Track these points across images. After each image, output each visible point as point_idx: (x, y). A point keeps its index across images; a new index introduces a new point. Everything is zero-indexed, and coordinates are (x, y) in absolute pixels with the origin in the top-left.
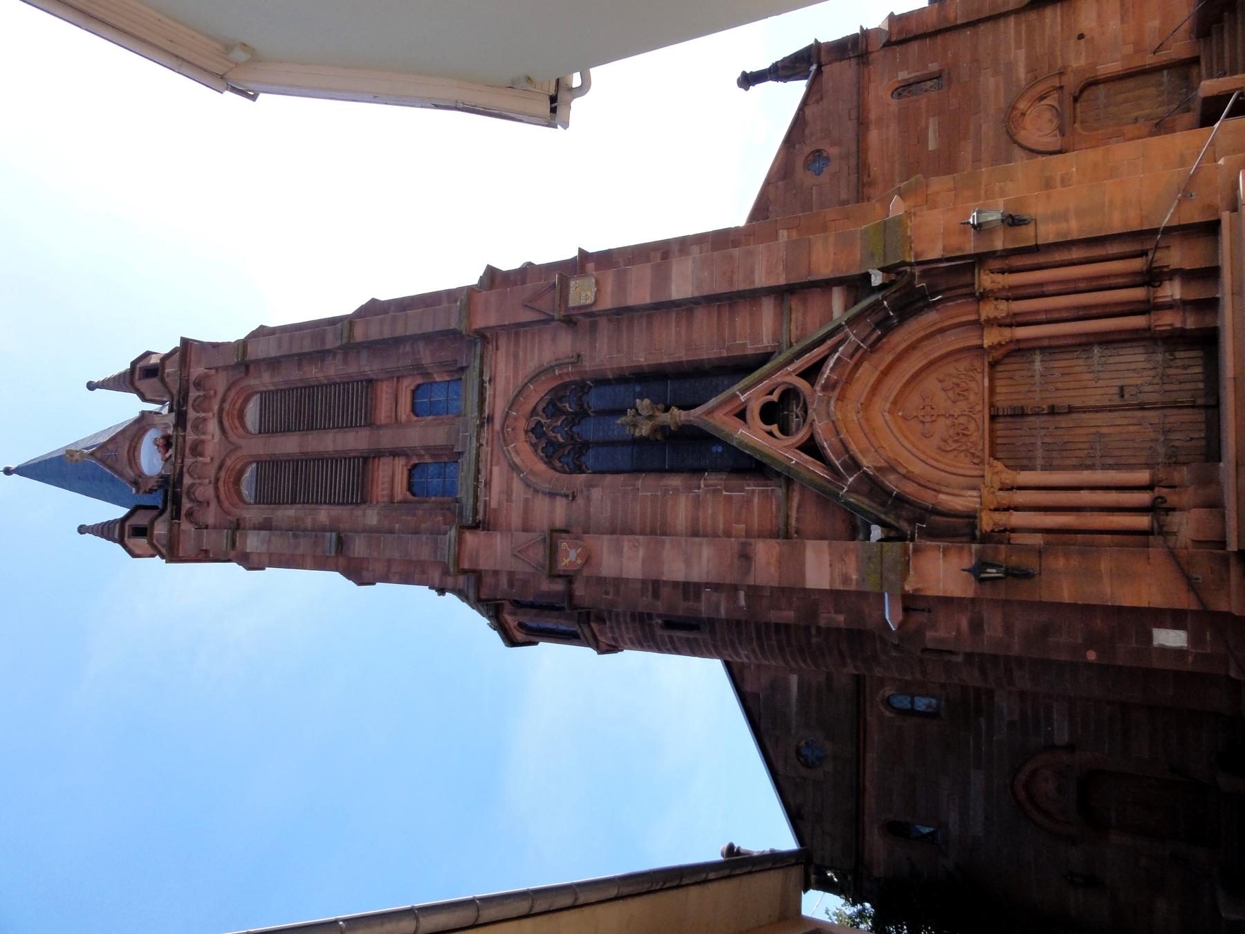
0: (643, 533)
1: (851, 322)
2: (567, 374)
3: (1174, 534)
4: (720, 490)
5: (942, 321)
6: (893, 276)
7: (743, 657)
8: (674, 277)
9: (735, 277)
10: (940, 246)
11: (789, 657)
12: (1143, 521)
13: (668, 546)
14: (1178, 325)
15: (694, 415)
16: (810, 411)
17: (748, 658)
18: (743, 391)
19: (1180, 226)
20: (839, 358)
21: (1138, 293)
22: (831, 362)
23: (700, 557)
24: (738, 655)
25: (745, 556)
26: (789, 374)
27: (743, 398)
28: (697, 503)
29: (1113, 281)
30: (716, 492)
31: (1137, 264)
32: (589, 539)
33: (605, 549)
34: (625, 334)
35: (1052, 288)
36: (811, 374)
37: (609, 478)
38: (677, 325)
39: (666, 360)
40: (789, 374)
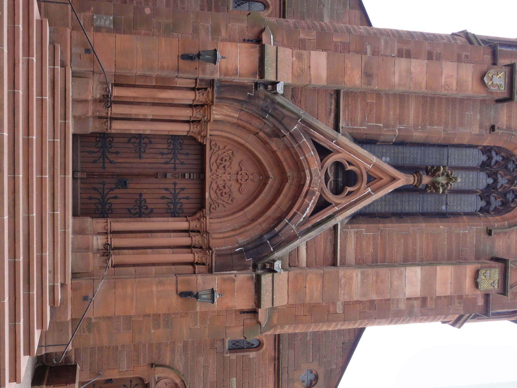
0: (440, 99)
1: (293, 238)
2: (498, 221)
4: (385, 126)
5: (234, 236)
7: (362, 29)
8: (419, 284)
9: (375, 278)
11: (332, 28)
12: (117, 92)
13: (424, 85)
16: (323, 177)
17: (360, 28)
18: (369, 195)
20: (303, 214)
21: (116, 242)
22: (308, 211)
23: (400, 76)
24: (366, 29)
25: (368, 75)
26: (337, 204)
27: (369, 190)
28: (401, 119)
30: (387, 126)
32: (482, 94)
33: (470, 83)
36: (322, 205)
38: (415, 251)
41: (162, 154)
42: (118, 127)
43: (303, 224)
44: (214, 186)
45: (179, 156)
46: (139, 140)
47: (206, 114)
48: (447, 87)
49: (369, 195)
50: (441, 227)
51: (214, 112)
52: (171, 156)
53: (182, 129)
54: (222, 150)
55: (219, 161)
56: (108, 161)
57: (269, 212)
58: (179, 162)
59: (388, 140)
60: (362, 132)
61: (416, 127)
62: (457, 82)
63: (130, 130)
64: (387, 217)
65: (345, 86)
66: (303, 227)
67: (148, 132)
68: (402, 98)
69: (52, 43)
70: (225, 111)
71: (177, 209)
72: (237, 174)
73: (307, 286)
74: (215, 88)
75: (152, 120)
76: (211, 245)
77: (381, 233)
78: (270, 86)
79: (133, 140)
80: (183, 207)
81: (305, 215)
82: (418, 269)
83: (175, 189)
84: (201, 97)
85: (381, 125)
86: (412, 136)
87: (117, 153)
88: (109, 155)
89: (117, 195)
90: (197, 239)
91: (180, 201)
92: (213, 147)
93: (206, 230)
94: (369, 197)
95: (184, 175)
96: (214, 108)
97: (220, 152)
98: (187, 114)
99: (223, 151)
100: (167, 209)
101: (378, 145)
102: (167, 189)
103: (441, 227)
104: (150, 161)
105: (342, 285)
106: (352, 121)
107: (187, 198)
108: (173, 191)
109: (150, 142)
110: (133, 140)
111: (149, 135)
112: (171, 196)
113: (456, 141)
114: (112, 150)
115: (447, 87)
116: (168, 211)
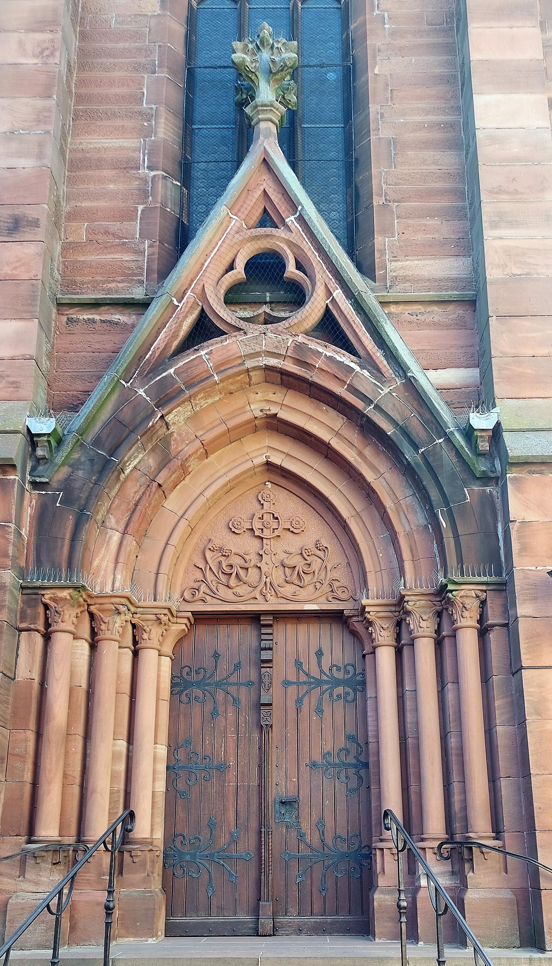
3: (23, 873)
6: (484, 446)
10: (530, 517)
13: (40, 103)
14: (382, 882)
15: (267, 141)
18: (301, 220)
19: (537, 889)
21: (435, 824)
23: (19, 155)
26: (329, 293)
28: (128, 166)
29: (456, 787)
30: (144, 194)
31: (480, 826)
34: (420, 41)
35: (450, 696)
36: (330, 328)
37: (179, 29)
39: (373, 108)
40: (329, 293)
41: (214, 713)
42: (149, 826)
43: (379, 370)
44: (288, 590)
48: (46, 53)
49: (301, 220)
50: (376, 71)
51: (108, 590)
52: (220, 696)
54: (204, 576)
55: (233, 581)
56: (233, 847)
57: (350, 455)
59: (178, 197)
60: (156, 250)
61: (147, 133)
62: (34, 31)
64: (357, 196)
65: (40, 277)
66: (383, 370)
67: (162, 751)
68: (77, 166)
70: (104, 565)
73: (531, 353)
74: (46, 583)
75: (130, 739)
76: (432, 591)
77: (394, 201)
78: (40, 452)
79: (181, 786)
81: (353, 365)
82: (479, 101)
83: (298, 684)
84: (69, 619)
85: (140, 208)
86: (165, 141)
87: (211, 826)
90: (422, 625)
94: (309, 228)
95: (264, 661)
96: (98, 589)
97: (210, 577)
98: (115, 659)
99: (208, 573)
100: (346, 701)
101: (188, 222)
102: (299, 701)
103: (376, 71)
104: (228, 742)
105: (526, 271)
106: (129, 275)
108: (305, 688)
109: (188, 742)
110: (181, 786)
111: (169, 746)
113: (179, 48)
115: (46, 53)
116: (350, 698)
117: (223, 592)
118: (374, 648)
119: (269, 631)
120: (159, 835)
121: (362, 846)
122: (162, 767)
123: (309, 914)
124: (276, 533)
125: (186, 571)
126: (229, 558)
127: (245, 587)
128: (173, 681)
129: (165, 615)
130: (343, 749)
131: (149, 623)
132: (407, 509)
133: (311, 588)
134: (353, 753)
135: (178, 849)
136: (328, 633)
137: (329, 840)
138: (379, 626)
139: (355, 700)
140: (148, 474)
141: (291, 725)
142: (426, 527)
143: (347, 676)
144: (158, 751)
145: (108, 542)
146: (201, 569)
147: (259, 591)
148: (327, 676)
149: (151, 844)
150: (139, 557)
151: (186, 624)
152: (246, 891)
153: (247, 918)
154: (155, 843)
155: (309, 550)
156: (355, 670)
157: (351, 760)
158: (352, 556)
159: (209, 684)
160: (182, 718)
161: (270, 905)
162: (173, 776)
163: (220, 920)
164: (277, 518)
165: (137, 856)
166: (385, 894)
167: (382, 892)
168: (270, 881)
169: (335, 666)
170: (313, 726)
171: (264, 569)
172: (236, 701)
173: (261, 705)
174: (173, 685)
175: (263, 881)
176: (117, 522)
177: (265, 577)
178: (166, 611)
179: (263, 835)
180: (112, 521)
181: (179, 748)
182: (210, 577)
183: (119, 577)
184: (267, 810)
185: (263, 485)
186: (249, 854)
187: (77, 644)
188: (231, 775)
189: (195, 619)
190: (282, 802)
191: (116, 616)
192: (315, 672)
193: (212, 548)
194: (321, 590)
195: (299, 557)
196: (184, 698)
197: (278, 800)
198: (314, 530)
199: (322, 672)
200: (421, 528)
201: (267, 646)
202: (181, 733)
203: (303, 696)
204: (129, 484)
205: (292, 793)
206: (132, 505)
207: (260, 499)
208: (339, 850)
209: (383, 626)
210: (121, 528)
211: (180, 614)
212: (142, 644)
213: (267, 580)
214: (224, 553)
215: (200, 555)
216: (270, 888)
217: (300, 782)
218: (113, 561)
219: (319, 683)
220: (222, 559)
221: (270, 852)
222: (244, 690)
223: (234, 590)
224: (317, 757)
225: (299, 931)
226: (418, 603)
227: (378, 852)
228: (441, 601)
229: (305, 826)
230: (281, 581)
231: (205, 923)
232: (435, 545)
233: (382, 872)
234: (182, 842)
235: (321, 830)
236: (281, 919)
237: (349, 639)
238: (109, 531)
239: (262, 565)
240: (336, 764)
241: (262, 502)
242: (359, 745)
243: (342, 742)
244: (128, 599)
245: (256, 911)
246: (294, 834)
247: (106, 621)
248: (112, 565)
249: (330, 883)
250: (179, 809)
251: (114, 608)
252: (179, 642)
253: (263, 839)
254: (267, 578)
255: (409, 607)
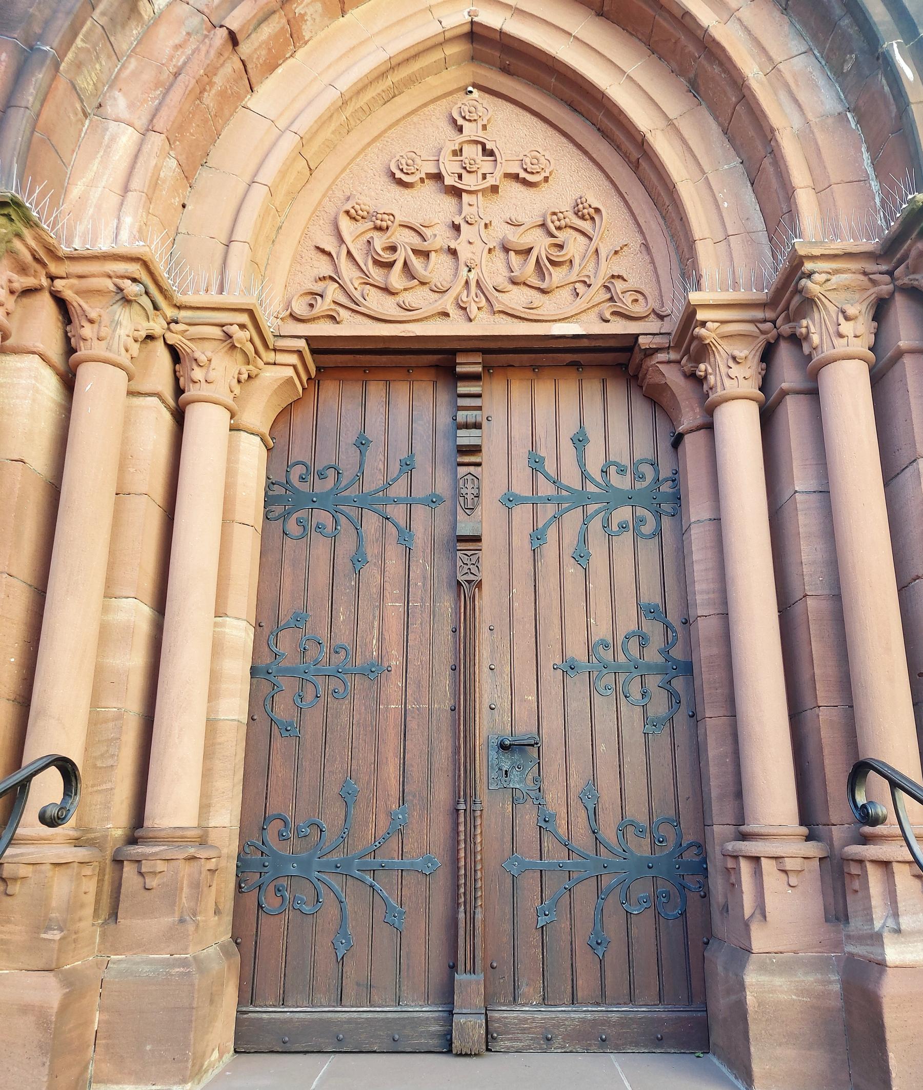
41: (358, 561)
44: (517, 298)
45: (373, 480)
46: (283, 682)
47: (109, 284)
52: (371, 522)
53: (229, 465)
55: (396, 279)
56: (394, 843)
58: (403, 481)
63: (212, 725)
67: (240, 633)
69: (460, 747)
70: (95, 195)
71: (639, 485)
72: (457, 193)
79: (283, 710)
80: (625, 461)
83: (535, 501)
87: (347, 798)
88: (365, 838)
89: (574, 792)
91: (598, 477)
92: (322, 306)
93: (763, 306)
97: (348, 272)
100: (637, 534)
102: (537, 537)
104: (388, 613)
107: (580, 441)
108: (550, 510)
109: (299, 620)
110: (283, 710)
112: (573, 520)
114: (332, 817)
116: (648, 528)
117: (376, 302)
118: (710, 411)
119: (474, 389)
120: (226, 818)
121: (684, 845)
122: (237, 669)
123: (567, 998)
124: (490, 181)
125: (297, 259)
126: (389, 233)
127: (424, 292)
128: (270, 493)
129: (242, 326)
130: (634, 634)
131: (207, 345)
132: (796, 81)
133: (566, 293)
134: (657, 640)
135: (271, 849)
136: (598, 399)
137: (609, 833)
138: (724, 355)
139: (658, 533)
140: (206, 10)
141: (523, 589)
142: (841, 117)
143: (639, 485)
144: (227, 630)
145: (108, 146)
146: (329, 254)
147: (452, 299)
148: (597, 485)
149: (202, 841)
150: (189, 207)
151: (295, 367)
152: (424, 947)
153: (423, 1011)
154: (213, 837)
155: (561, 215)
156: (657, 472)
157: (653, 655)
158: (654, 225)
159: (346, 501)
160: (287, 568)
161: (478, 983)
162: (266, 687)
163: (365, 1015)
164: (491, 153)
165: (154, 873)
166: (772, 973)
167: (763, 968)
168: (478, 924)
169: (615, 464)
170: (568, 586)
171: (465, 254)
172: (405, 536)
173: (458, 541)
174: (269, 501)
175: (461, 925)
176: (131, 106)
177: (466, 269)
178: (244, 318)
179: (462, 819)
180: (119, 104)
181: (280, 629)
182: (348, 272)
183: (128, 220)
184: (480, 761)
185: (462, 93)
186: (430, 860)
187: (19, 365)
188: (393, 686)
189: (318, 369)
190: (503, 747)
191: (118, 308)
192: (571, 477)
193: (352, 211)
194: (586, 298)
195: (539, 232)
196: (292, 526)
197: (495, 742)
198: (571, 179)
199: (585, 476)
200: (830, 121)
201: (471, 420)
202: (286, 598)
203: (547, 526)
204: (162, 30)
205: (524, 728)
206: (165, 76)
207: (456, 116)
208: (632, 853)
209: (737, 353)
210: (141, 121)
211: (282, 343)
212: (191, 392)
213: (472, 275)
214: (378, 222)
215: (329, 228)
216: (478, 940)
217: (543, 703)
218: (118, 189)
219: (580, 499)
220: (376, 234)
221: (479, 857)
222: (420, 513)
223: (400, 299)
224: (577, 651)
225: (546, 1041)
226: (834, 279)
227: (745, 867)
228: (890, 273)
229: (554, 798)
230: (501, 279)
231: (329, 1022)
232: (866, 155)
233: (758, 916)
234: (280, 834)
235: (591, 807)
236: (504, 1014)
237: (641, 411)
238: (112, 125)
239: (460, 245)
240: (620, 666)
241: (460, 121)
242: (667, 626)
243: (628, 621)
244: (146, 265)
245: (447, 995)
246: (528, 817)
247: (93, 315)
248: (115, 199)
249: (614, 928)
250: (277, 761)
251: (112, 287)
252: (285, 414)
253: (462, 828)
254: (470, 271)
255: (813, 287)
